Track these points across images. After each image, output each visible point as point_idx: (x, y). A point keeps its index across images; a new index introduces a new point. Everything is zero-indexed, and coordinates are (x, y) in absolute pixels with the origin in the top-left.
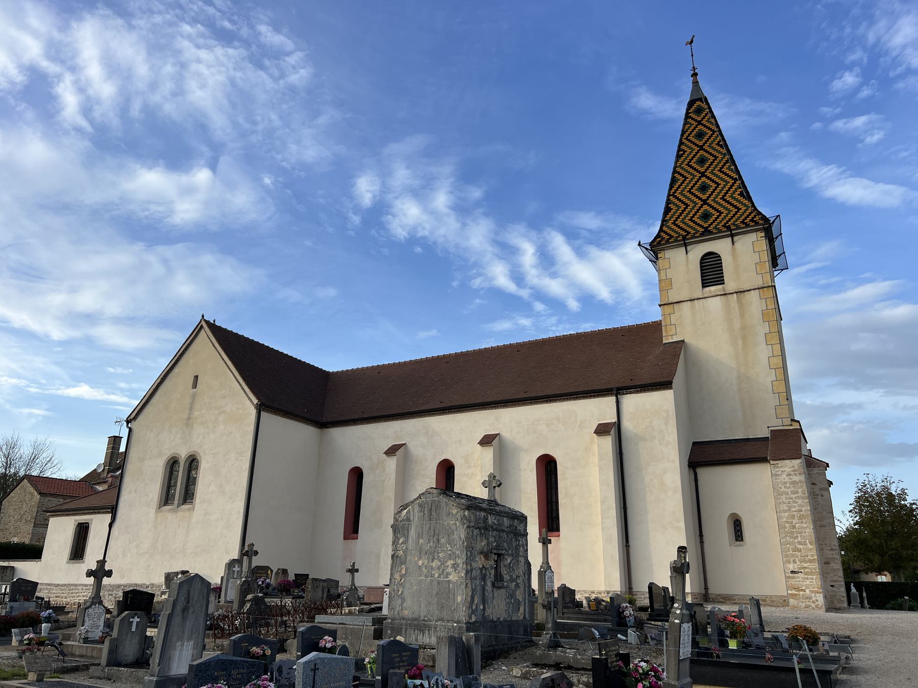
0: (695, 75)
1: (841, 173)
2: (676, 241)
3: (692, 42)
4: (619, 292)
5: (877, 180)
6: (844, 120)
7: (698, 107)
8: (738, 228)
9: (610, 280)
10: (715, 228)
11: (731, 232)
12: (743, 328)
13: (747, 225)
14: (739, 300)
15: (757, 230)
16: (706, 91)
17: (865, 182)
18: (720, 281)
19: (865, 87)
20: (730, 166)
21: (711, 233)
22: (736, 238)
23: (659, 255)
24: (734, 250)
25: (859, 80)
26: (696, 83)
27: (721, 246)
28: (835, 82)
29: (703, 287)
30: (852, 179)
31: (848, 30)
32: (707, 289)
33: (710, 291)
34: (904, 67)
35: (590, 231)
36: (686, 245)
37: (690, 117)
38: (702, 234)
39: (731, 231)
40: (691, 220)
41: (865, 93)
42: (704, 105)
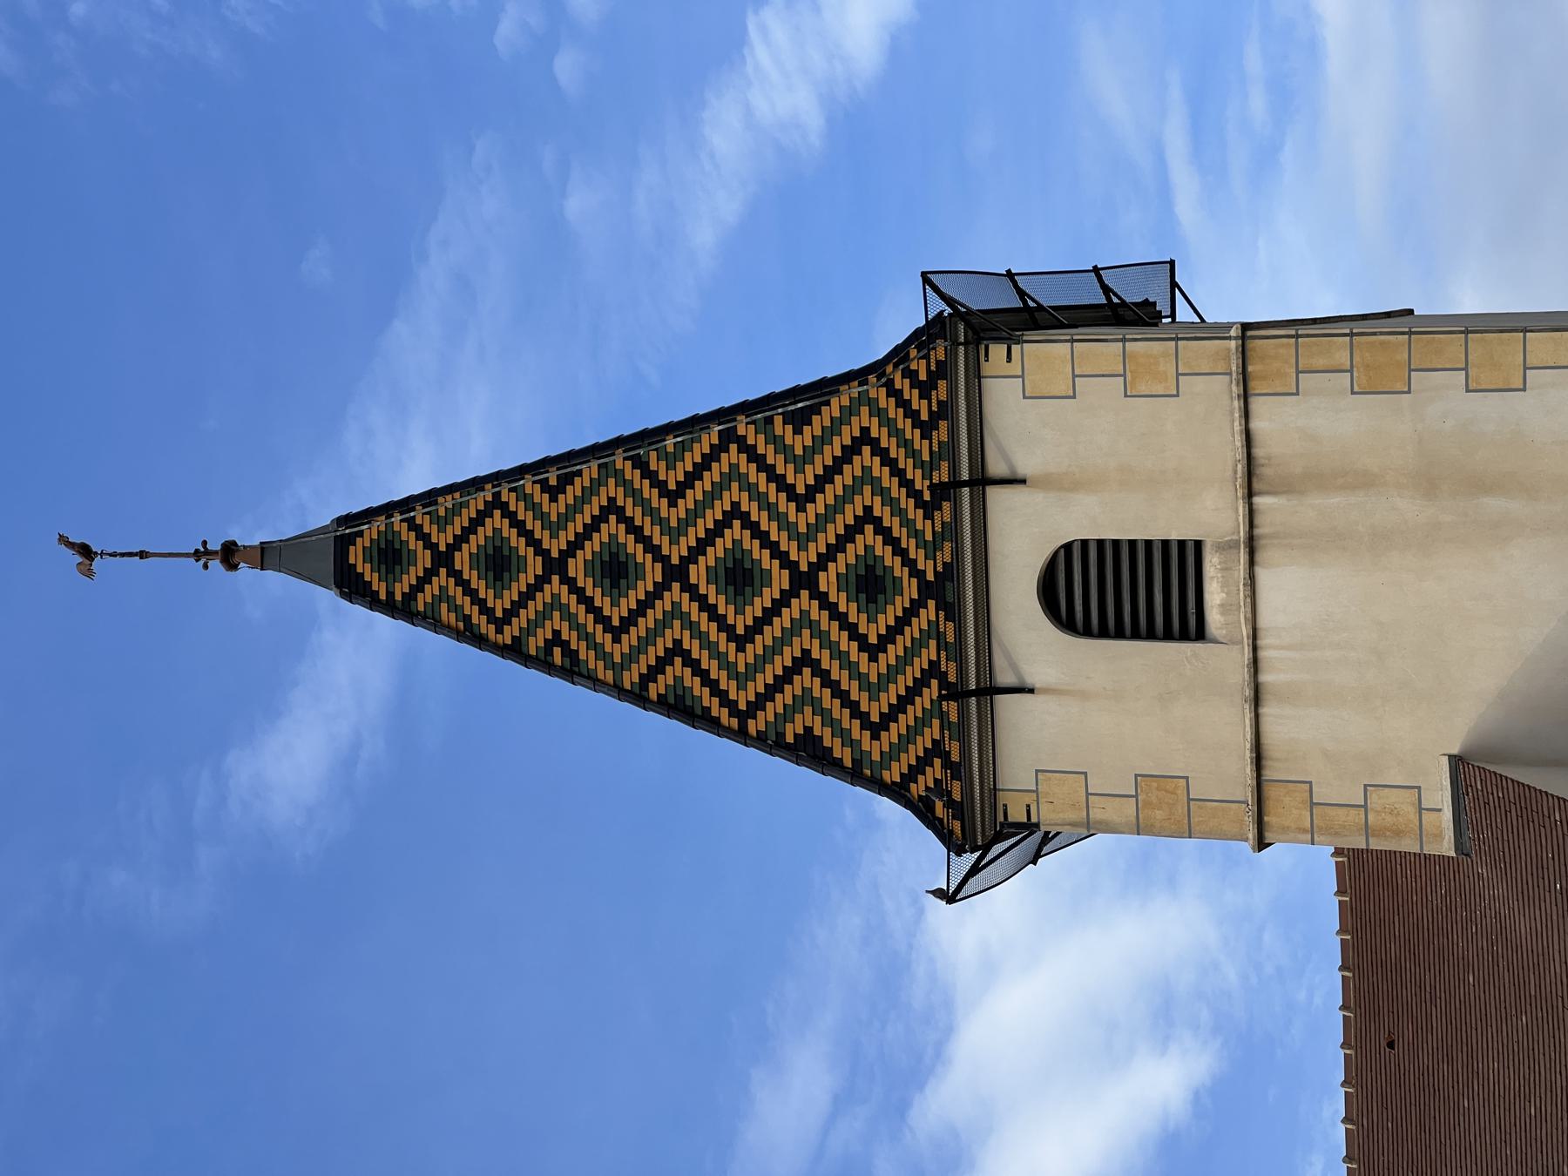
3: (85, 551)
4: (1163, 1012)
7: (370, 559)
9: (1101, 1043)
10: (932, 549)
11: (963, 484)
12: (1428, 483)
13: (945, 411)
14: (1286, 487)
15: (976, 375)
18: (1183, 560)
20: (663, 455)
21: (950, 573)
22: (996, 467)
23: (1017, 815)
24: (1047, 482)
26: (266, 556)
29: (1200, 635)
32: (1214, 618)
33: (1225, 608)
35: (842, 1102)
36: (990, 691)
37: (410, 597)
38: (952, 610)
39: (957, 484)
40: (873, 652)
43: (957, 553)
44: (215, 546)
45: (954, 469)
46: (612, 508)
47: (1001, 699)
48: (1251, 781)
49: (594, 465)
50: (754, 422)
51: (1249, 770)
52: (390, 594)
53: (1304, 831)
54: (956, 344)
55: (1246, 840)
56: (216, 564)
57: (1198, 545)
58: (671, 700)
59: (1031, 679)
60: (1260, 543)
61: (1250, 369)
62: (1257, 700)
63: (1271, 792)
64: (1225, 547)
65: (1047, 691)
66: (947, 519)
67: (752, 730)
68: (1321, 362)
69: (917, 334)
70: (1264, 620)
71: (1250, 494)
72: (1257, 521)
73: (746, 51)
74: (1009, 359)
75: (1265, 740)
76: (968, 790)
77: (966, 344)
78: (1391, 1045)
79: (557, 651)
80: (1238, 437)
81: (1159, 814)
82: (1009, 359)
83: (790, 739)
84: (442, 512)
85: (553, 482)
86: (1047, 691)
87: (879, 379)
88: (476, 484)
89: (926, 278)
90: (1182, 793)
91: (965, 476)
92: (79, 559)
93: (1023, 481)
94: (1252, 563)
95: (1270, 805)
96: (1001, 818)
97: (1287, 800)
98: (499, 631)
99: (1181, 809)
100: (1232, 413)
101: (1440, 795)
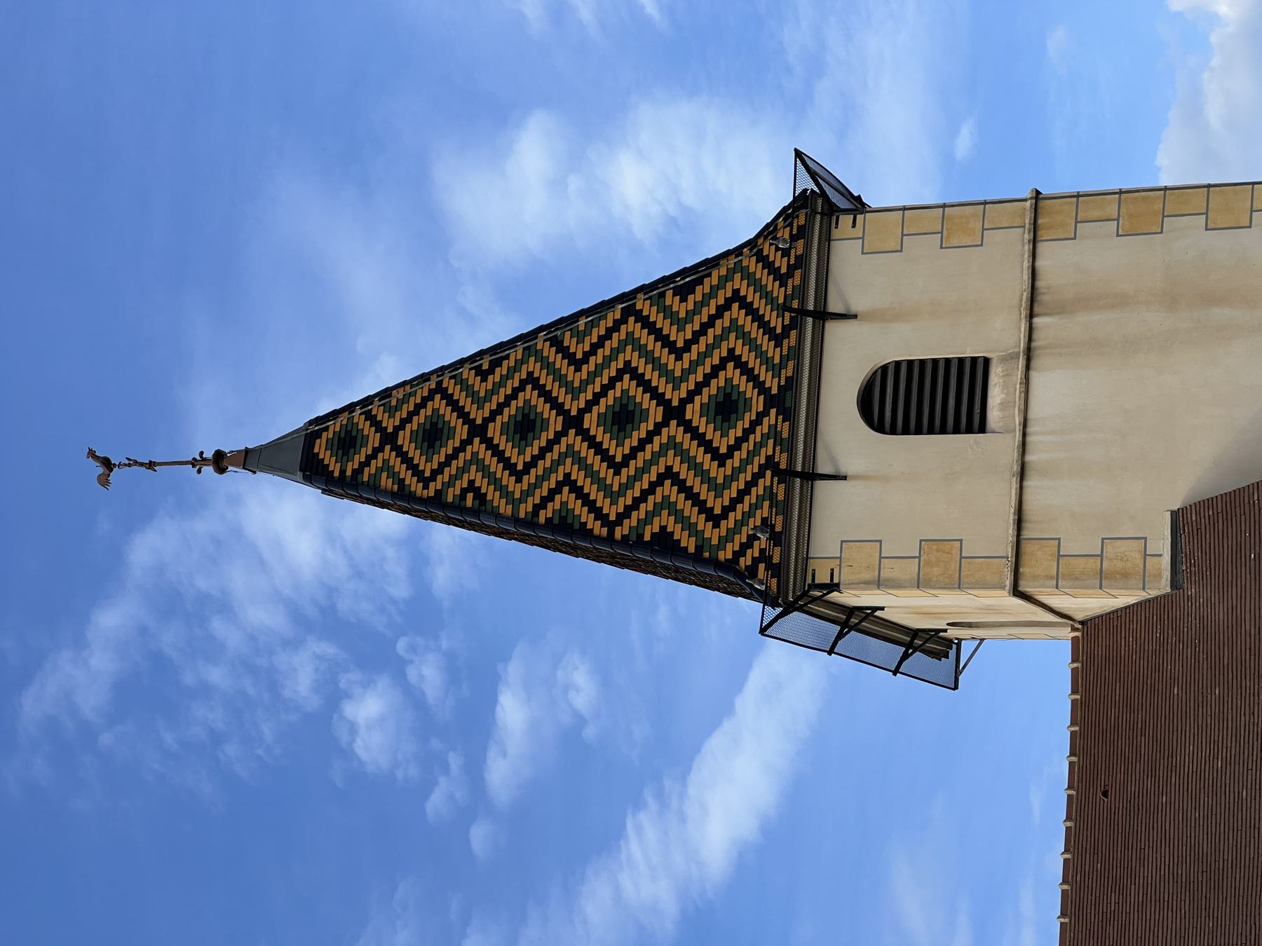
0: (220, 461)
1: (663, 804)
2: (784, 508)
3: (107, 464)
5: (723, 709)
6: (492, 753)
7: (330, 456)
8: (802, 291)
10: (776, 370)
11: (812, 314)
12: (1171, 300)
13: (801, 262)
14: (1061, 309)
15: (827, 239)
16: (291, 420)
17: (716, 742)
18: (974, 372)
19: (412, 673)
21: (791, 385)
22: (834, 306)
23: (822, 578)
24: (874, 316)
25: (383, 683)
26: (251, 459)
27: (849, 359)
28: (359, 748)
29: (982, 429)
30: (693, 779)
31: (217, 675)
33: (1003, 406)
34: (390, 552)
36: (811, 476)
37: (357, 472)
38: (788, 414)
41: (428, 674)
42: (335, 426)
43: (798, 369)
44: (209, 454)
45: (803, 301)
46: (531, 380)
47: (820, 484)
48: (1011, 538)
49: (520, 350)
50: (650, 298)
51: (1011, 530)
52: (343, 472)
53: (1051, 578)
54: (814, 212)
55: (1003, 588)
56: (209, 470)
57: (987, 361)
58: (556, 521)
59: (844, 470)
60: (1035, 353)
61: (1040, 221)
62: (1022, 475)
63: (1027, 548)
64: (1010, 358)
65: (857, 477)
66: (793, 343)
67: (618, 536)
68: (1095, 214)
69: (785, 209)
70: (1031, 415)
71: (1031, 316)
72: (1035, 336)
73: (622, 843)
74: (854, 225)
75: (1026, 507)
76: (785, 555)
77: (822, 214)
78: (1105, 794)
79: (470, 496)
80: (1025, 272)
81: (936, 571)
82: (854, 225)
83: (647, 537)
84: (394, 403)
85: (485, 367)
86: (857, 477)
87: (751, 250)
88: (424, 378)
89: (798, 154)
90: (956, 552)
91: (811, 307)
92: (101, 470)
93: (855, 317)
94: (1028, 368)
95: (1025, 559)
96: (809, 581)
97: (1039, 553)
98: (426, 487)
99: (954, 566)
100: (1023, 256)
101: (1163, 545)
